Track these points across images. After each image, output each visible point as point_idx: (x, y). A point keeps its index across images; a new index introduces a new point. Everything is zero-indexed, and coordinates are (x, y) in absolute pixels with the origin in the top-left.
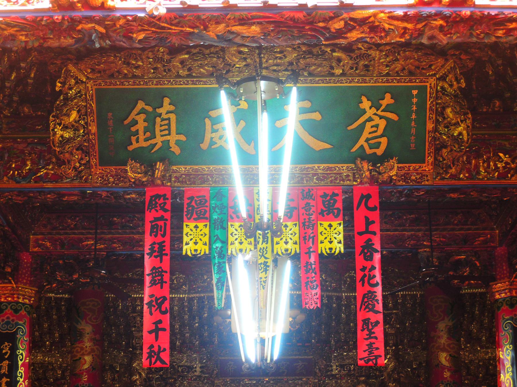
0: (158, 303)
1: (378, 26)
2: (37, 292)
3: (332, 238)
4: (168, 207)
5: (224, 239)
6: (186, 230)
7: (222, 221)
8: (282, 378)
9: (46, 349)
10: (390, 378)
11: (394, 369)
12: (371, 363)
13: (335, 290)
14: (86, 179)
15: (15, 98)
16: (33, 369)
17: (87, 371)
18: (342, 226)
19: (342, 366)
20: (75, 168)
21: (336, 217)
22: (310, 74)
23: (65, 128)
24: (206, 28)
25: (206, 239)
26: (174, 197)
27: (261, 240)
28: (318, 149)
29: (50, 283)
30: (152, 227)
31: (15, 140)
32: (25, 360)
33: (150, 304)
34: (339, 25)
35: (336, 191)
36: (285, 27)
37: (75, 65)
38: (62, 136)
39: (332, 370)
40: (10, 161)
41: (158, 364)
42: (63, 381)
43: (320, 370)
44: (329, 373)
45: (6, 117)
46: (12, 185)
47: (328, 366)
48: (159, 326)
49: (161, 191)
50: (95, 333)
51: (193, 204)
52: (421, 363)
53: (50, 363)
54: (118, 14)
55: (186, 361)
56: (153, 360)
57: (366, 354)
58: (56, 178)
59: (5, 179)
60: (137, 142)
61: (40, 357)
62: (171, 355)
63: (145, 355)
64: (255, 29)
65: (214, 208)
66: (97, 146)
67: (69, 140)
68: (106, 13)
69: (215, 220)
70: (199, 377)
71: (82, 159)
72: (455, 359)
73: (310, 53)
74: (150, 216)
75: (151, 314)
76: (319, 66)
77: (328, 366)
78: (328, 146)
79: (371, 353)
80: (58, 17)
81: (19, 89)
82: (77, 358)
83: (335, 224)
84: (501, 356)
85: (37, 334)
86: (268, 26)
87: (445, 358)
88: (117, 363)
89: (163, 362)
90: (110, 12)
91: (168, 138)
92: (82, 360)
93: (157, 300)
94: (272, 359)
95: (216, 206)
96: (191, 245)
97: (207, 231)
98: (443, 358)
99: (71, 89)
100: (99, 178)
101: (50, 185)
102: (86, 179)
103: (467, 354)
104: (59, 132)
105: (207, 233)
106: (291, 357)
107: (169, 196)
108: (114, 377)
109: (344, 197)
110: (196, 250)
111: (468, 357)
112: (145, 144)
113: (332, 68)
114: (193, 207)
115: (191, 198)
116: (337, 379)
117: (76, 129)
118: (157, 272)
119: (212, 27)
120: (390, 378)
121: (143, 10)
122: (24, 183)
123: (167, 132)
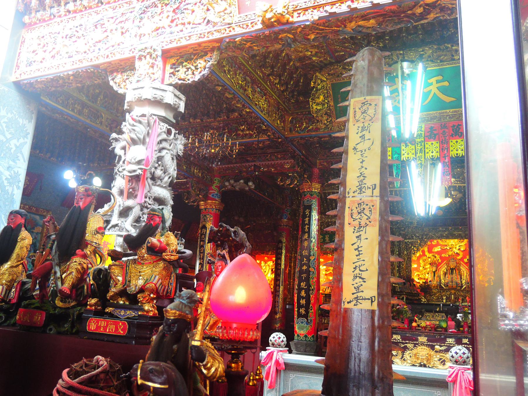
1: (444, 6)
2: (322, 186)
14: (331, 129)
15: (295, 93)
20: (325, 124)
22: (441, 61)
23: (318, 104)
24: (345, 26)
27: (419, 152)
31: (297, 114)
34: (419, 10)
36: (389, 17)
37: (320, 73)
38: (316, 109)
40: (296, 123)
45: (293, 103)
46: (297, 134)
54: (296, 25)
64: (372, 21)
67: (320, 110)
68: (290, 26)
70: (416, 227)
71: (328, 119)
73: (440, 49)
76: (445, 55)
78: (453, 99)
80: (267, 32)
81: (297, 89)
86: (379, 18)
96: (406, 155)
99: (319, 85)
101: (314, 133)
102: (331, 129)
104: (315, 107)
105: (414, 148)
113: (453, 56)
117: (324, 105)
119: (348, 25)
121: (308, 20)
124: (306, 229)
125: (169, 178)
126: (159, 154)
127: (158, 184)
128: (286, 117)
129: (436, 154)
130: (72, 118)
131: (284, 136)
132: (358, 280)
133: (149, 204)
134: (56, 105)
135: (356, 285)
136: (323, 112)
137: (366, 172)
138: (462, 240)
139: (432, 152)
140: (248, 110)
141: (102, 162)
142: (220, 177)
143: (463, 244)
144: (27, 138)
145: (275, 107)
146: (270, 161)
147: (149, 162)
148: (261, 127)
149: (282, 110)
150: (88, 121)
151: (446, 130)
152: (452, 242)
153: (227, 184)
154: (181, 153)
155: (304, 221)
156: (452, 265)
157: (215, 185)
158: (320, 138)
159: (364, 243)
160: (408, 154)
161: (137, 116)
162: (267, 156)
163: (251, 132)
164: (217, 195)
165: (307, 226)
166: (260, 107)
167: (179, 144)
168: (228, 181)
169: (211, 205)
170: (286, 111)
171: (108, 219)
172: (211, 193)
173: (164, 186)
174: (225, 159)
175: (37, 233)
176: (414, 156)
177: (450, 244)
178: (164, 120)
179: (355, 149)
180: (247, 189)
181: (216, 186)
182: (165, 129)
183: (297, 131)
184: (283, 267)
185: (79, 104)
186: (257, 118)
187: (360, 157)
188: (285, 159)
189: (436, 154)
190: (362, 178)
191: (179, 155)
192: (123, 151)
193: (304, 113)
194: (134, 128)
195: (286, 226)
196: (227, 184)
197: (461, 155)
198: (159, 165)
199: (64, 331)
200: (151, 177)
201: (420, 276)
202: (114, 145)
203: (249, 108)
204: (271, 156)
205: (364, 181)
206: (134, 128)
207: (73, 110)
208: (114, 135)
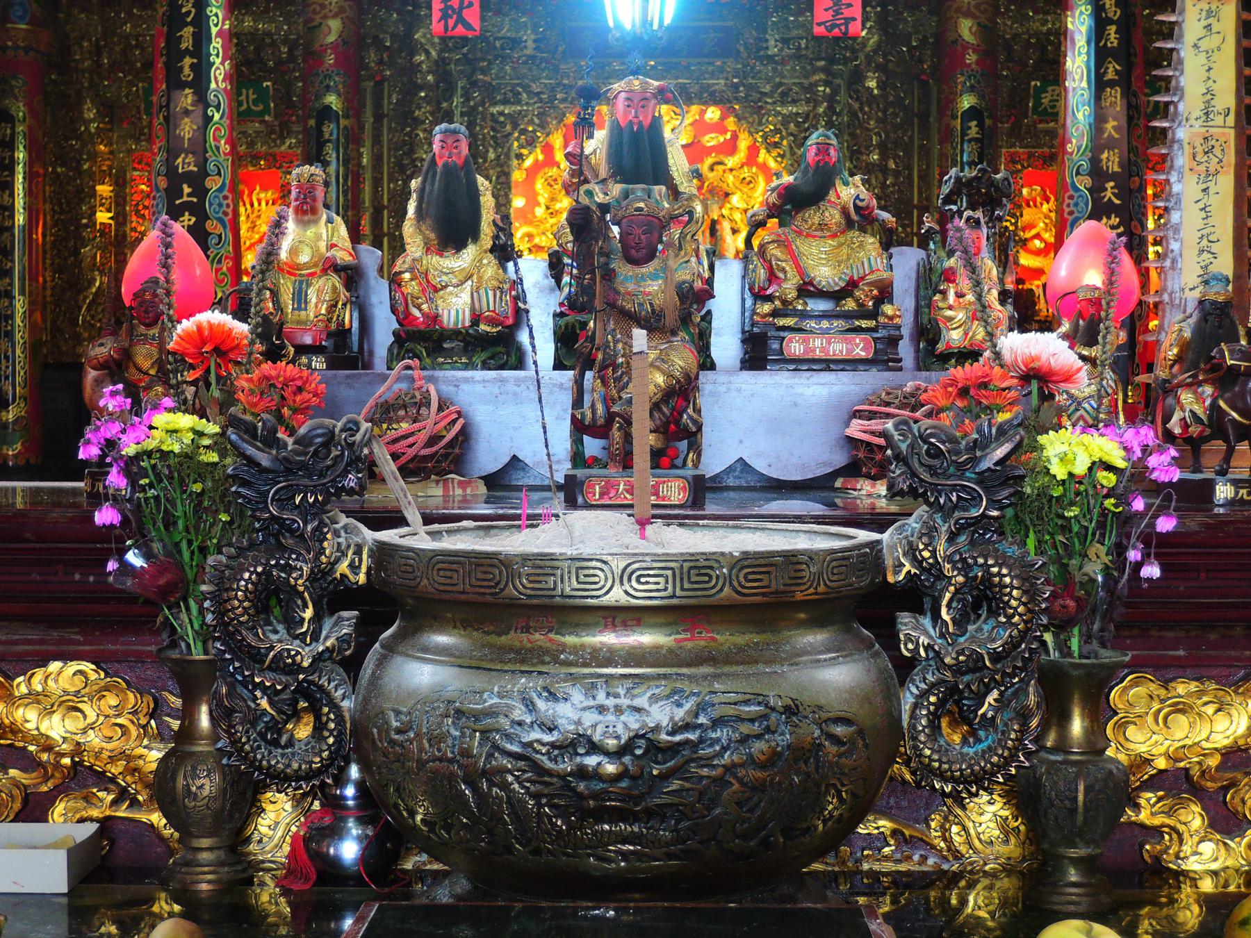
8: (678, 60)
9: (258, 8)
10: (869, 64)
11: (879, 45)
12: (836, 30)
16: (237, 45)
17: (334, 46)
19: (785, 41)
32: (223, 24)
39: (767, 48)
41: (460, 29)
42: (291, 66)
43: (746, 48)
44: (762, 53)
47: (760, 40)
52: (925, 38)
53: (269, 34)
55: (508, 30)
56: (451, 23)
57: (828, 16)
61: (248, 23)
62: (483, 19)
63: (436, 15)
70: (533, 57)
72: (987, 31)
77: (760, 40)
79: (837, 13)
82: (315, 23)
84: (1070, 26)
87: (970, 29)
88: (386, 32)
89: (468, 26)
90: (697, 568)
92: (323, 27)
94: (661, 26)
98: (966, 29)
103: (1009, 23)
106: (701, 24)
108: (382, 59)
111: (1011, 28)
116: (776, 63)
120: (869, 64)
124: (187, 70)
132: (1205, 255)
135: (1203, 264)
137: (1214, 86)
155: (173, 40)
159: (1213, 200)
165: (188, 61)
179: (1196, 46)
184: (20, 219)
187: (1205, 61)
190: (1209, 97)
195: (27, 49)
201: (537, 240)
205: (1213, 103)
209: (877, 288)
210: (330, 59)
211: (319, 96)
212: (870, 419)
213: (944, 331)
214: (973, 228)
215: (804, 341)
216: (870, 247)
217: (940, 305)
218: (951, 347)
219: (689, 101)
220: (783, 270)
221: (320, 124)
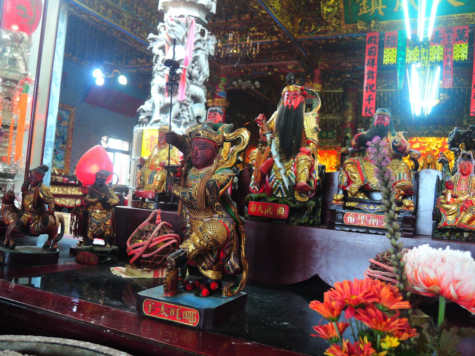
0: (370, 87)
3: (461, 52)
4: (377, 42)
5: (403, 55)
6: (385, 52)
7: (403, 47)
13: (467, 86)
14: (339, 32)
17: (350, 122)
18: (467, 46)
20: (334, 26)
21: (464, 41)
23: (328, 7)
25: (395, 56)
26: (380, 37)
28: (456, 6)
29: (327, 82)
30: (369, 52)
31: (307, 16)
33: (367, 88)
35: (465, 28)
38: (327, 11)
40: (305, 26)
45: (303, 5)
46: (306, 37)
48: (371, 97)
49: (374, 34)
50: (353, 106)
51: (390, 39)
53: (335, 120)
58: (326, 32)
59: (303, 34)
60: (363, 11)
65: (400, 41)
66: (343, 15)
67: (330, 13)
69: (400, 47)
71: (337, 22)
74: (368, 47)
75: (367, 92)
83: (463, 45)
85: (330, 107)
91: (378, 7)
93: (370, 85)
95: (401, 40)
96: (388, 59)
97: (396, 52)
100: (345, 30)
101: (322, 36)
102: (339, 32)
104: (325, 9)
105: (396, 53)
107: (377, 36)
109: (470, 31)
110: (390, 62)
112: (366, 12)
114: (389, 41)
115: (389, 37)
118: (370, 73)
122: (311, 35)
123: (377, 5)
125: (204, 77)
126: (195, 54)
127: (194, 82)
128: (296, 19)
129: (439, 58)
130: (97, 19)
131: (293, 38)
133: (188, 102)
134: (83, 5)
136: (333, 14)
138: (440, 138)
139: (436, 56)
140: (264, 12)
141: (119, 62)
142: (226, 76)
143: (440, 142)
144: (61, 38)
145: (287, 10)
146: (274, 62)
147: (188, 62)
148: (274, 28)
149: (293, 13)
150: (112, 22)
151: (451, 35)
152: (431, 140)
153: (235, 83)
154: (212, 54)
156: (429, 160)
157: (221, 84)
158: (328, 40)
160: (412, 57)
161: (176, 17)
162: (271, 57)
163: (261, 34)
164: (223, 93)
166: (275, 9)
167: (211, 44)
168: (236, 80)
169: (218, 103)
170: (297, 13)
171: (150, 115)
172: (218, 91)
173: (200, 84)
174: (247, 59)
175: (64, 127)
176: (418, 59)
177: (429, 141)
178: (199, 21)
180: (253, 88)
181: (223, 85)
182: (199, 30)
183: (306, 33)
185: (104, 4)
186: (271, 19)
188: (289, 60)
189: (439, 58)
191: (210, 55)
192: (161, 51)
193: (313, 15)
194: (173, 28)
196: (235, 83)
197: (464, 59)
198: (196, 65)
199: (305, 223)
200: (188, 76)
202: (152, 44)
203: (266, 10)
204: (275, 57)
206: (173, 28)
207: (98, 11)
208: (151, 35)
209: (402, 189)
210: (349, 125)
211: (346, 134)
212: (374, 269)
213: (443, 216)
214: (466, 160)
215: (355, 216)
216: (402, 168)
217: (442, 201)
218: (447, 225)
219: (441, 137)
220: (354, 178)
221: (345, 140)
